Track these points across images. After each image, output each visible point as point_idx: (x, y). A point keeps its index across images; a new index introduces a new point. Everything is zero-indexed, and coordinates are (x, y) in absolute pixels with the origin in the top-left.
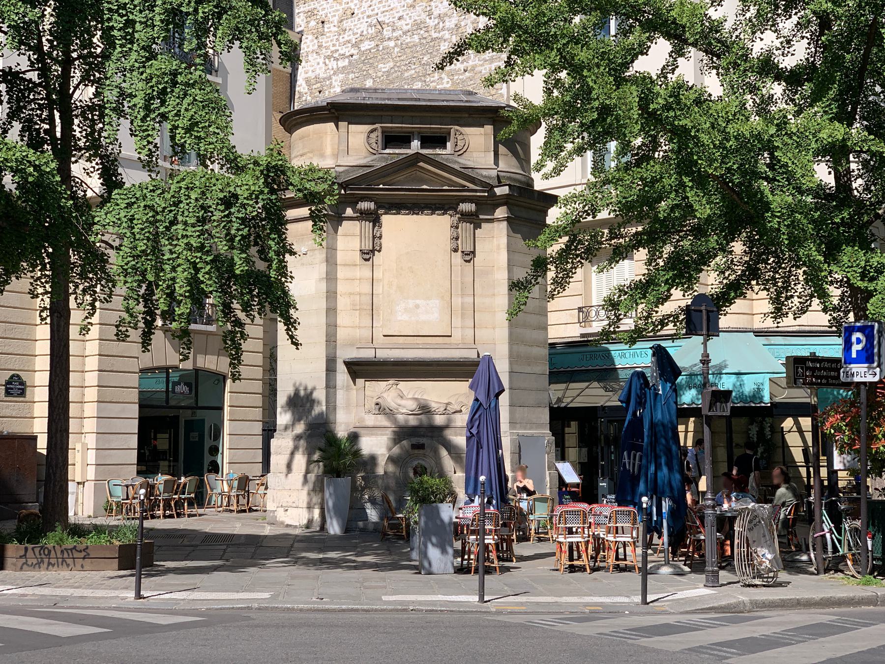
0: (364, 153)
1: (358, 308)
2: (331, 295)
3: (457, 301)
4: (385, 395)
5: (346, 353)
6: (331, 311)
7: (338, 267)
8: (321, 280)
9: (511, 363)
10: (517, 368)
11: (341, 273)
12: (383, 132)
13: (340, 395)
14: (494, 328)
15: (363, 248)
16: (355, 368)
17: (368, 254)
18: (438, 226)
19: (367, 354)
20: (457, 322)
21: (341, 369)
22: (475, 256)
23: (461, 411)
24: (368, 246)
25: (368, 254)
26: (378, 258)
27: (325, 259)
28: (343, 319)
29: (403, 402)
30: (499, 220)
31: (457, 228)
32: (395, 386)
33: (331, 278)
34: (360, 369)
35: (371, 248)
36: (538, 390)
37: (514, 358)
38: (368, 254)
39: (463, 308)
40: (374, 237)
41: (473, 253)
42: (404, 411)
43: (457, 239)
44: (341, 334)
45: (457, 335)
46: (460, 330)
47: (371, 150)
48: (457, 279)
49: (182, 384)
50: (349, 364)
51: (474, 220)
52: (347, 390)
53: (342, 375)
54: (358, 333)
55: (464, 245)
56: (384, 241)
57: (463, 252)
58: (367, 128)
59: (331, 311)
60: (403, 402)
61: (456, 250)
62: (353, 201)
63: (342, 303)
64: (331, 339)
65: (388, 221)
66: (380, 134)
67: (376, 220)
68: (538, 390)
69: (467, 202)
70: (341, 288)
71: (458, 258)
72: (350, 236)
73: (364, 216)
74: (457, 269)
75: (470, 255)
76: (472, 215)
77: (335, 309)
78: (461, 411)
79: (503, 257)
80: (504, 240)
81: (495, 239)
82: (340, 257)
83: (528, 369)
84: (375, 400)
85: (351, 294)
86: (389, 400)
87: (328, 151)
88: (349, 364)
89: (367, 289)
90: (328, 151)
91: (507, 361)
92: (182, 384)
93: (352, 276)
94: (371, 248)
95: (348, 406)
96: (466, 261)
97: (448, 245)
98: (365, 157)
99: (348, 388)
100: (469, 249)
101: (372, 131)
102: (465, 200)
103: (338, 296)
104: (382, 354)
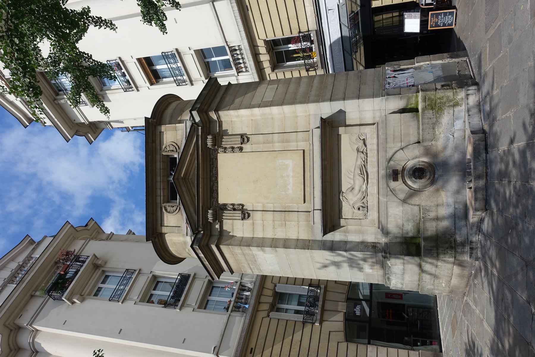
0: (179, 215)
1: (284, 222)
2: (275, 244)
3: (278, 146)
4: (351, 202)
5: (318, 235)
6: (286, 244)
7: (255, 236)
8: (263, 251)
9: (323, 101)
10: (328, 95)
11: (259, 234)
12: (168, 202)
13: (354, 238)
14: (297, 117)
15: (240, 218)
16: (329, 225)
17: (245, 214)
18: (225, 161)
19: (318, 216)
20: (293, 145)
21: (329, 237)
22: (246, 134)
23: (364, 140)
24: (238, 214)
25: (244, 214)
26: (248, 207)
27: (248, 247)
28: (293, 234)
29: (357, 188)
30: (219, 117)
31: (225, 148)
32: (344, 195)
33: (261, 243)
34: (331, 219)
35: (240, 212)
36: (347, 79)
37: (319, 99)
38: (245, 214)
39: (283, 142)
40: (234, 210)
41: (242, 136)
42: (364, 187)
43: (233, 148)
44: (304, 236)
45: (303, 145)
46: (299, 143)
47: (177, 211)
48: (261, 147)
49: (355, 310)
50: (325, 233)
51: (219, 136)
52: (348, 233)
53: (336, 236)
54: (303, 223)
55: (237, 142)
56: (236, 202)
57: (242, 144)
58: (166, 214)
59: (286, 244)
60: (357, 188)
61: (241, 149)
62: (208, 227)
63: (280, 234)
64: (306, 245)
65: (222, 200)
66: (167, 204)
67: (224, 207)
68: (347, 79)
69: (208, 140)
70: (269, 234)
71: (247, 147)
72: (234, 226)
73: (218, 217)
74: (255, 147)
75: (244, 138)
76: (215, 137)
77: (286, 240)
78: (364, 140)
79: (243, 112)
80: (232, 113)
81: (235, 119)
82: (248, 234)
83: (330, 88)
84: (356, 211)
85: (274, 228)
86: (355, 199)
87: (182, 239)
88: (325, 233)
89: (270, 215)
90: (182, 239)
91: (321, 104)
92: (355, 310)
93: (261, 226)
94: (240, 212)
95: (360, 232)
96: (248, 141)
97: (237, 155)
98: (182, 215)
99: (346, 232)
100: (239, 139)
101: (166, 210)
102: (205, 143)
103: (276, 237)
104: (318, 204)
